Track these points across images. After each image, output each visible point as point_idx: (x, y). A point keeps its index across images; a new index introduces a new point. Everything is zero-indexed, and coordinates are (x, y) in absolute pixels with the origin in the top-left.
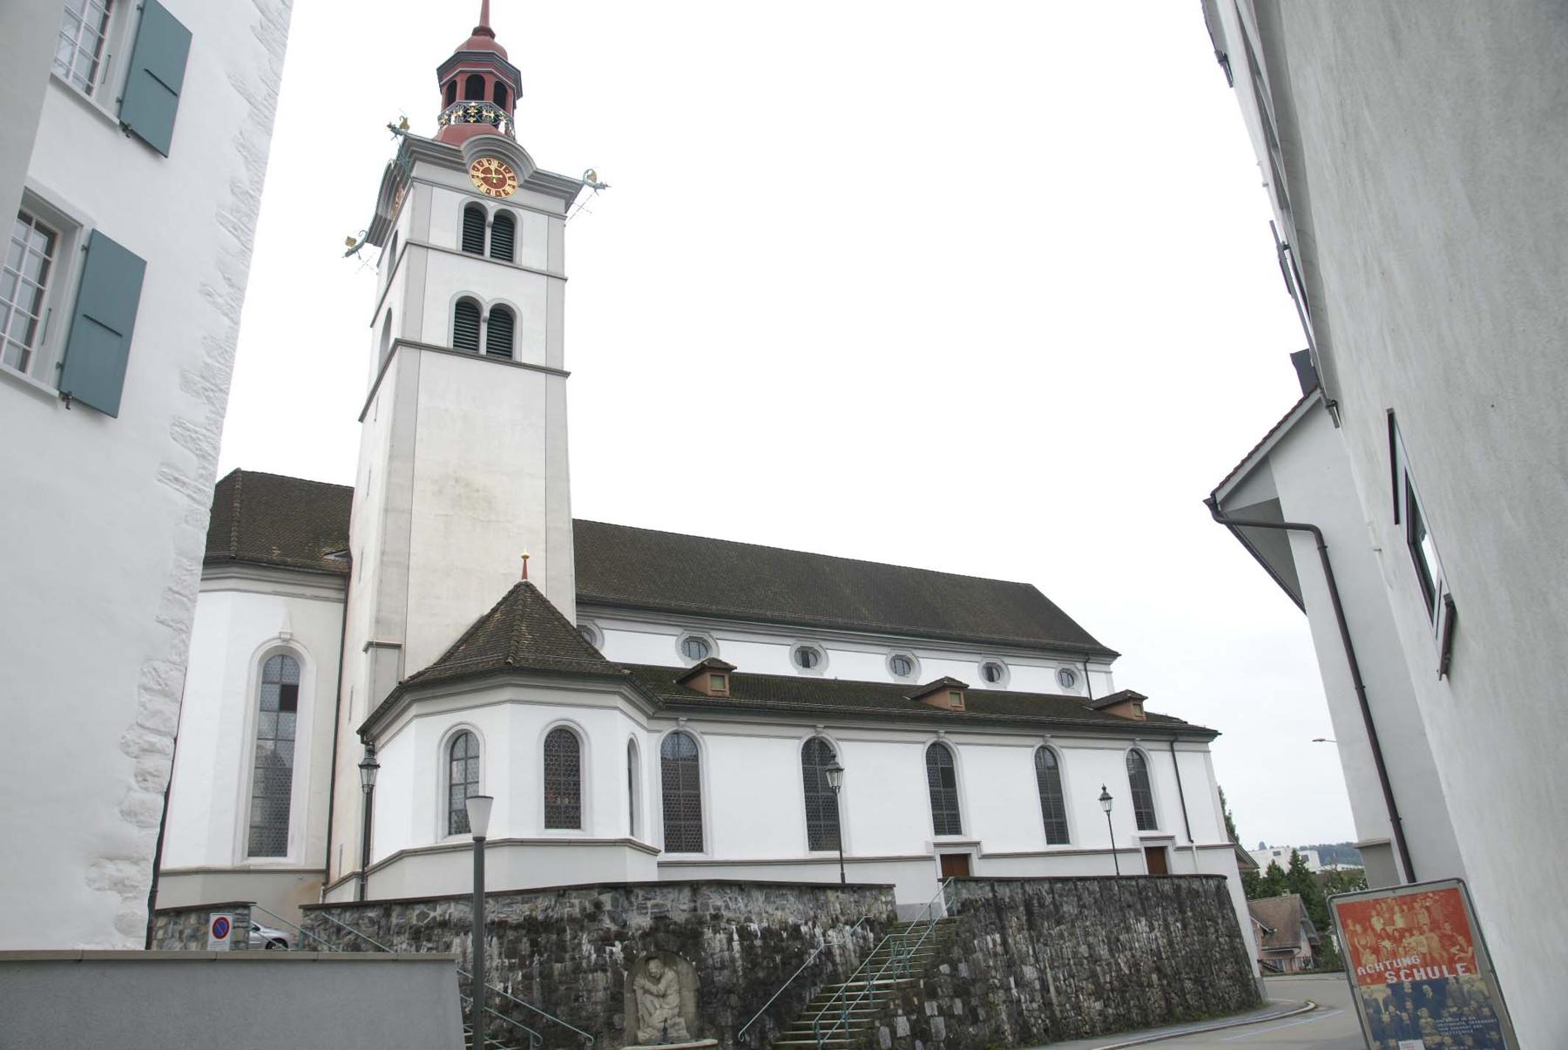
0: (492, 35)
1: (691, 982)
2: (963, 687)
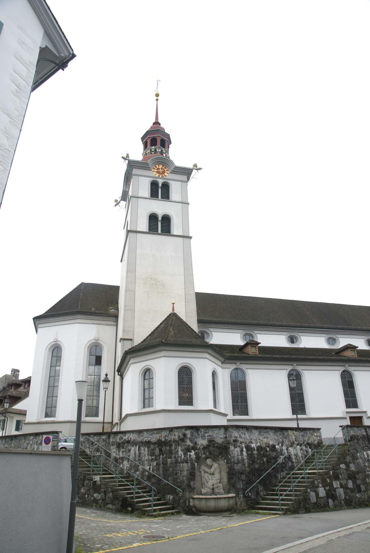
0: (160, 124)
1: (225, 468)
2: (355, 347)
